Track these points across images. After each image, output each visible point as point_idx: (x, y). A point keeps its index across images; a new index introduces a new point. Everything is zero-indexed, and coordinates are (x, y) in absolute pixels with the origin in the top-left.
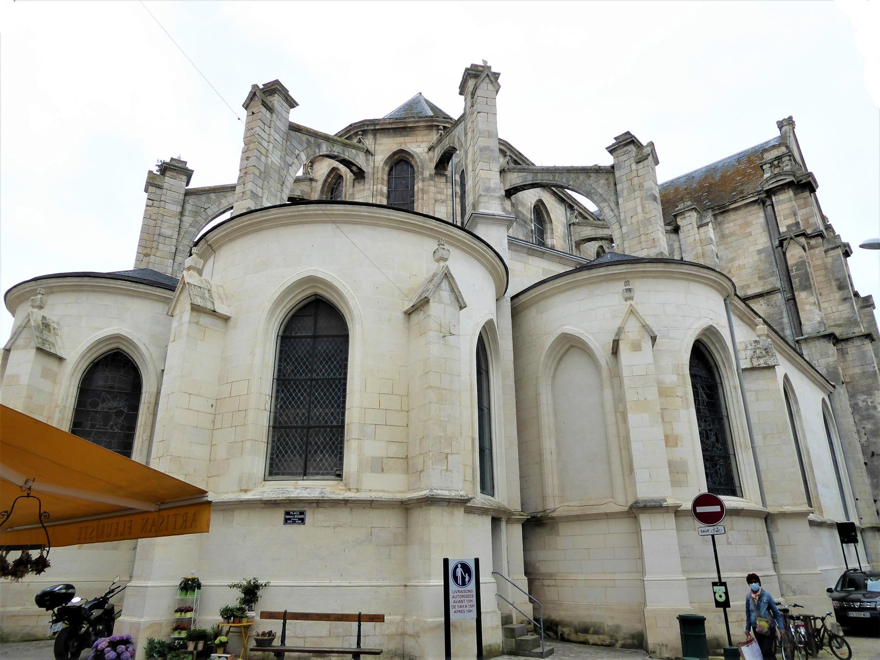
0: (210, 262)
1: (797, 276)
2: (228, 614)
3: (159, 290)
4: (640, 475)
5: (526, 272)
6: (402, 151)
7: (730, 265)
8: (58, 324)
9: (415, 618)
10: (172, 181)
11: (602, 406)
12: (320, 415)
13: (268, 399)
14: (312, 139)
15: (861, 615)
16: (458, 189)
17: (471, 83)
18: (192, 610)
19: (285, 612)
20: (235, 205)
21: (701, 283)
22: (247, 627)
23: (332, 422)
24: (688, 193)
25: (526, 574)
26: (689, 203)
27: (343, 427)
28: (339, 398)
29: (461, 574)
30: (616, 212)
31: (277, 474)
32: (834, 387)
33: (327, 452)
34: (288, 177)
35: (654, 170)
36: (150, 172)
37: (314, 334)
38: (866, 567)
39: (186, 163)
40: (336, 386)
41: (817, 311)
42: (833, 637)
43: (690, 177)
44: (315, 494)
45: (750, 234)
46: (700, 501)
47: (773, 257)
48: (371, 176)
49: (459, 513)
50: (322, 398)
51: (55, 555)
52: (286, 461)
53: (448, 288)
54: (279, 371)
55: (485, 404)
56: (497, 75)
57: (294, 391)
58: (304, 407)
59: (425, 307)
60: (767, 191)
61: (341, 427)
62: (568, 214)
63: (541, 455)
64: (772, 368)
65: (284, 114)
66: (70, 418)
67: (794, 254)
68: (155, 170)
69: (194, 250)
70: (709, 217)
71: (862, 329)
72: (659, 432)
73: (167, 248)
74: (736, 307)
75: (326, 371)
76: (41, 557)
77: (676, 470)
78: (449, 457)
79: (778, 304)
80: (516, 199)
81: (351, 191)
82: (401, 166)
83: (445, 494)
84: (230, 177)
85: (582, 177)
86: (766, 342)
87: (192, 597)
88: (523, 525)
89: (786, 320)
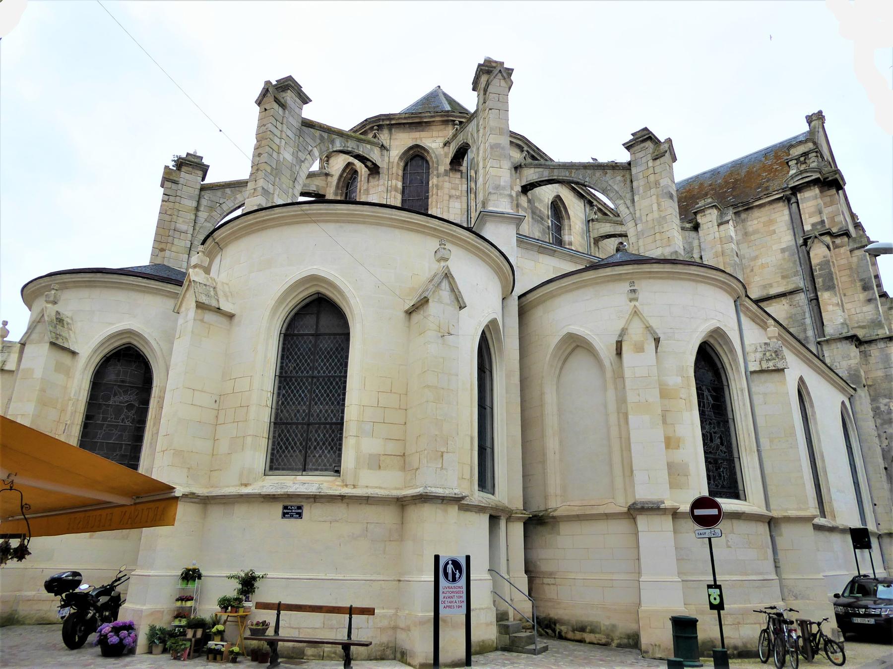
0: (217, 261)
1: (820, 276)
2: (225, 604)
3: (169, 286)
4: (639, 476)
5: (534, 270)
6: (417, 146)
7: (752, 264)
8: (72, 319)
9: (407, 612)
11: (605, 406)
12: (321, 411)
13: (269, 395)
14: (325, 135)
15: (866, 621)
17: (484, 79)
18: (192, 599)
19: (279, 604)
20: (246, 202)
21: (709, 284)
22: (244, 618)
23: (332, 419)
24: (712, 189)
25: (526, 572)
26: (710, 200)
27: (342, 424)
28: (339, 395)
29: (452, 570)
31: (277, 469)
32: (855, 389)
33: (326, 448)
34: (301, 173)
35: (671, 167)
36: (166, 167)
37: (316, 330)
38: (881, 573)
40: (337, 383)
41: (840, 312)
42: (828, 642)
43: (715, 173)
44: (312, 489)
45: (774, 232)
46: (700, 503)
47: (796, 256)
48: (385, 171)
50: (322, 395)
51: (36, 544)
53: (448, 288)
54: (282, 368)
55: (488, 403)
56: (510, 72)
57: (295, 387)
58: (305, 404)
61: (341, 424)
63: (544, 455)
65: (297, 110)
66: (82, 411)
67: (818, 252)
68: (171, 165)
70: (730, 214)
72: (659, 434)
73: (182, 243)
74: (748, 308)
75: (327, 368)
77: (676, 474)
78: (445, 455)
79: (801, 304)
80: (532, 195)
81: (365, 187)
82: (414, 160)
83: (440, 491)
84: (242, 172)
85: (598, 173)
86: (775, 344)
87: (193, 586)
88: (525, 524)
89: (808, 321)
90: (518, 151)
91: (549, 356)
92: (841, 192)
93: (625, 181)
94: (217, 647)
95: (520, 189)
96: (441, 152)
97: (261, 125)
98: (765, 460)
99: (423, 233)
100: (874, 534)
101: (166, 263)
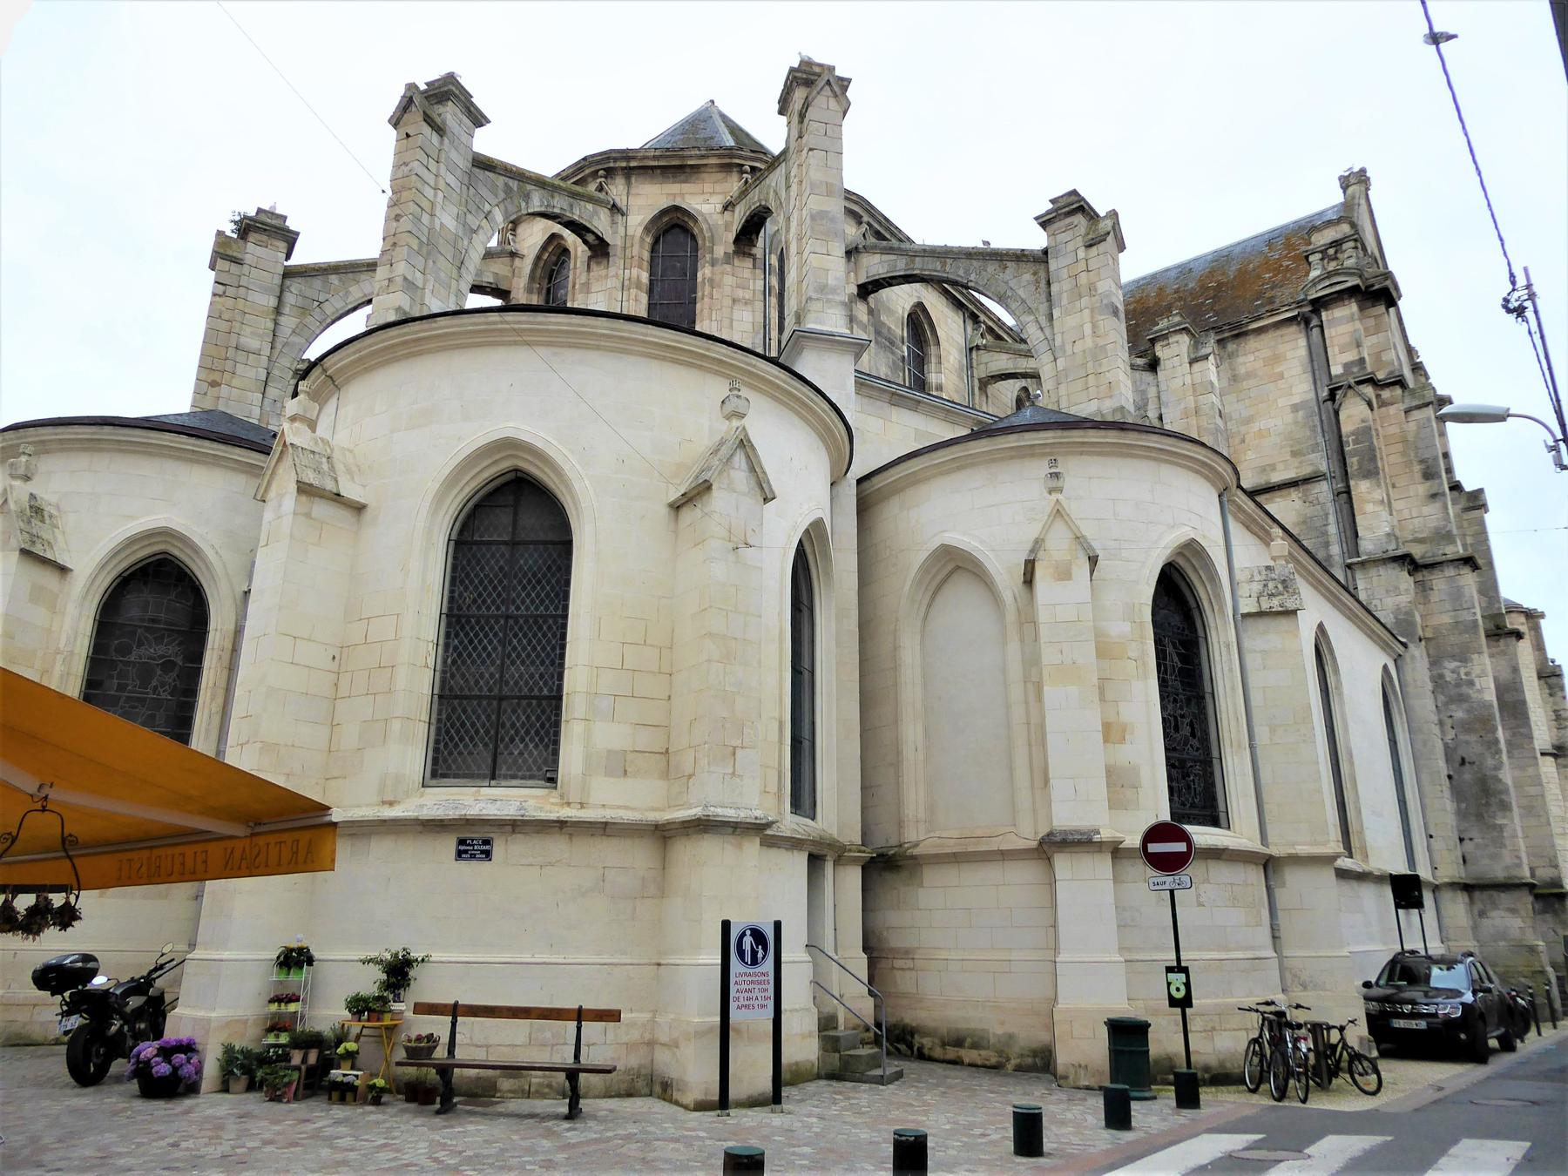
0: (331, 405)
2: (359, 1006)
3: (237, 450)
4: (1059, 788)
5: (886, 434)
6: (676, 208)
7: (1243, 429)
10: (259, 251)
11: (1004, 671)
12: (521, 676)
14: (514, 184)
15: (1412, 1024)
16: (775, 282)
17: (799, 94)
18: (297, 1000)
19: (456, 1005)
22: (391, 1029)
23: (541, 690)
24: (1180, 299)
25: (865, 949)
26: (1177, 319)
28: (553, 649)
29: (750, 946)
30: (1048, 331)
31: (444, 776)
32: (1405, 645)
33: (532, 740)
35: (1116, 261)
36: (220, 233)
37: (512, 537)
38: (1436, 948)
39: (284, 218)
40: (550, 628)
41: (1385, 515)
42: (1356, 1057)
43: (1184, 270)
45: (1281, 376)
46: (1156, 833)
47: (1317, 418)
48: (619, 252)
49: (752, 846)
50: (524, 649)
51: (87, 901)
52: (460, 753)
53: (744, 465)
54: (451, 600)
55: (806, 664)
56: (844, 83)
57: (476, 635)
59: (705, 498)
60: (1315, 302)
62: (969, 329)
63: (899, 753)
64: (1291, 613)
65: (464, 138)
67: (1353, 413)
68: (229, 229)
69: (302, 386)
70: (1210, 345)
71: (1458, 550)
73: (252, 372)
74: (1240, 508)
75: (533, 602)
76: (67, 903)
77: (1119, 783)
78: (739, 753)
80: (877, 301)
82: (665, 237)
83: (730, 814)
84: (369, 247)
85: (992, 267)
86: (1284, 568)
87: (297, 978)
89: (1332, 529)
91: (909, 583)
92: (1392, 310)
93: (1037, 281)
94: (346, 1080)
96: (719, 220)
99: (700, 367)
100: (1429, 884)
101: (221, 408)
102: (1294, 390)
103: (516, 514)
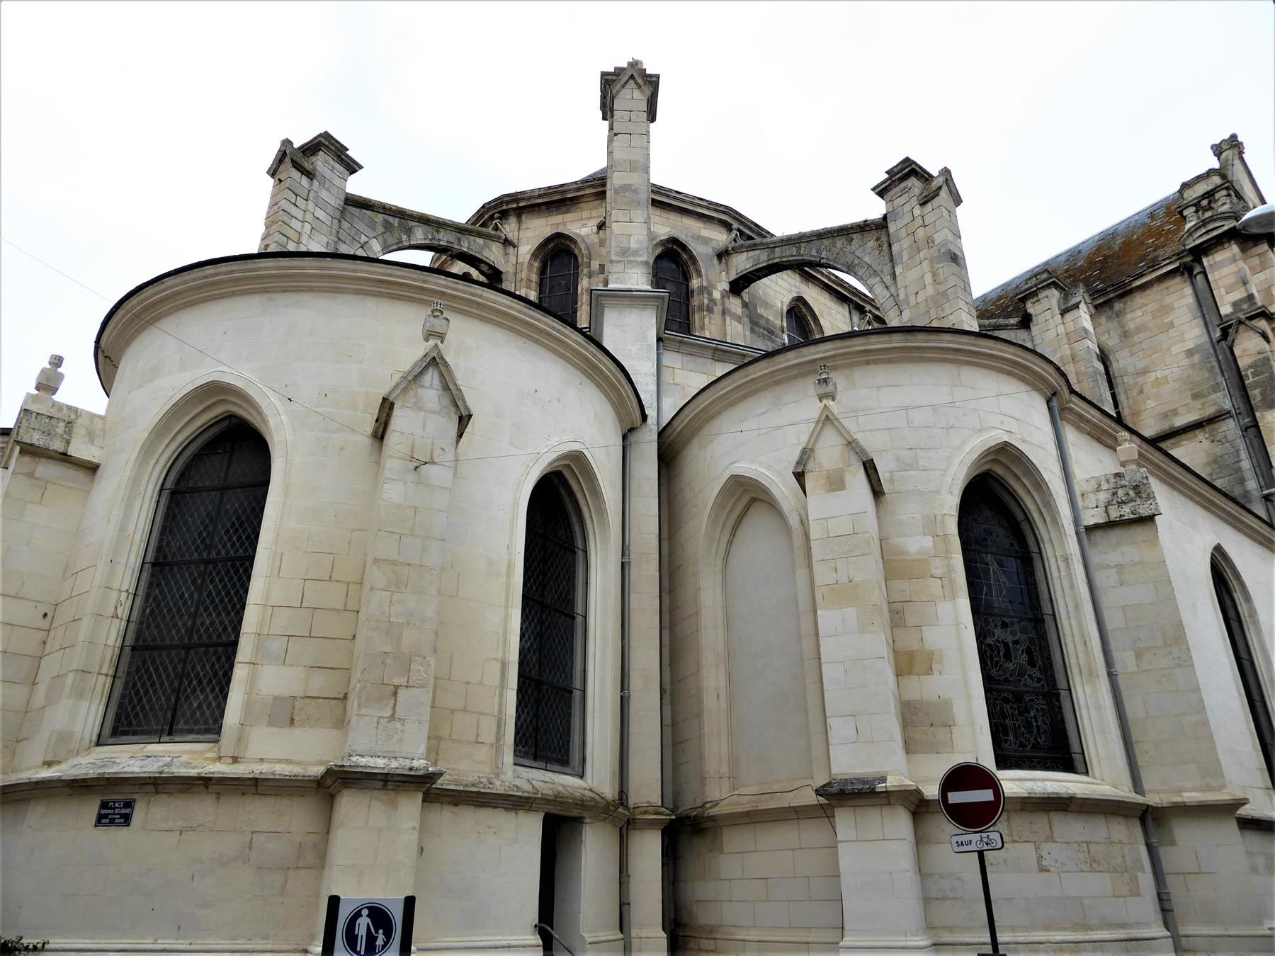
1: (1256, 385)
6: (558, 236)
7: (1140, 380)
12: (212, 623)
14: (395, 222)
24: (1070, 276)
35: (952, 214)
43: (1074, 253)
45: (1172, 325)
47: (1213, 359)
49: (411, 806)
53: (437, 383)
54: (159, 549)
65: (337, 181)
67: (1248, 347)
74: (1081, 417)
77: (918, 723)
78: (402, 693)
79: (1230, 438)
85: (840, 243)
89: (1246, 464)
90: (724, 230)
95: (727, 287)
97: (274, 204)
98: (1125, 694)
102: (1187, 336)
103: (230, 462)
